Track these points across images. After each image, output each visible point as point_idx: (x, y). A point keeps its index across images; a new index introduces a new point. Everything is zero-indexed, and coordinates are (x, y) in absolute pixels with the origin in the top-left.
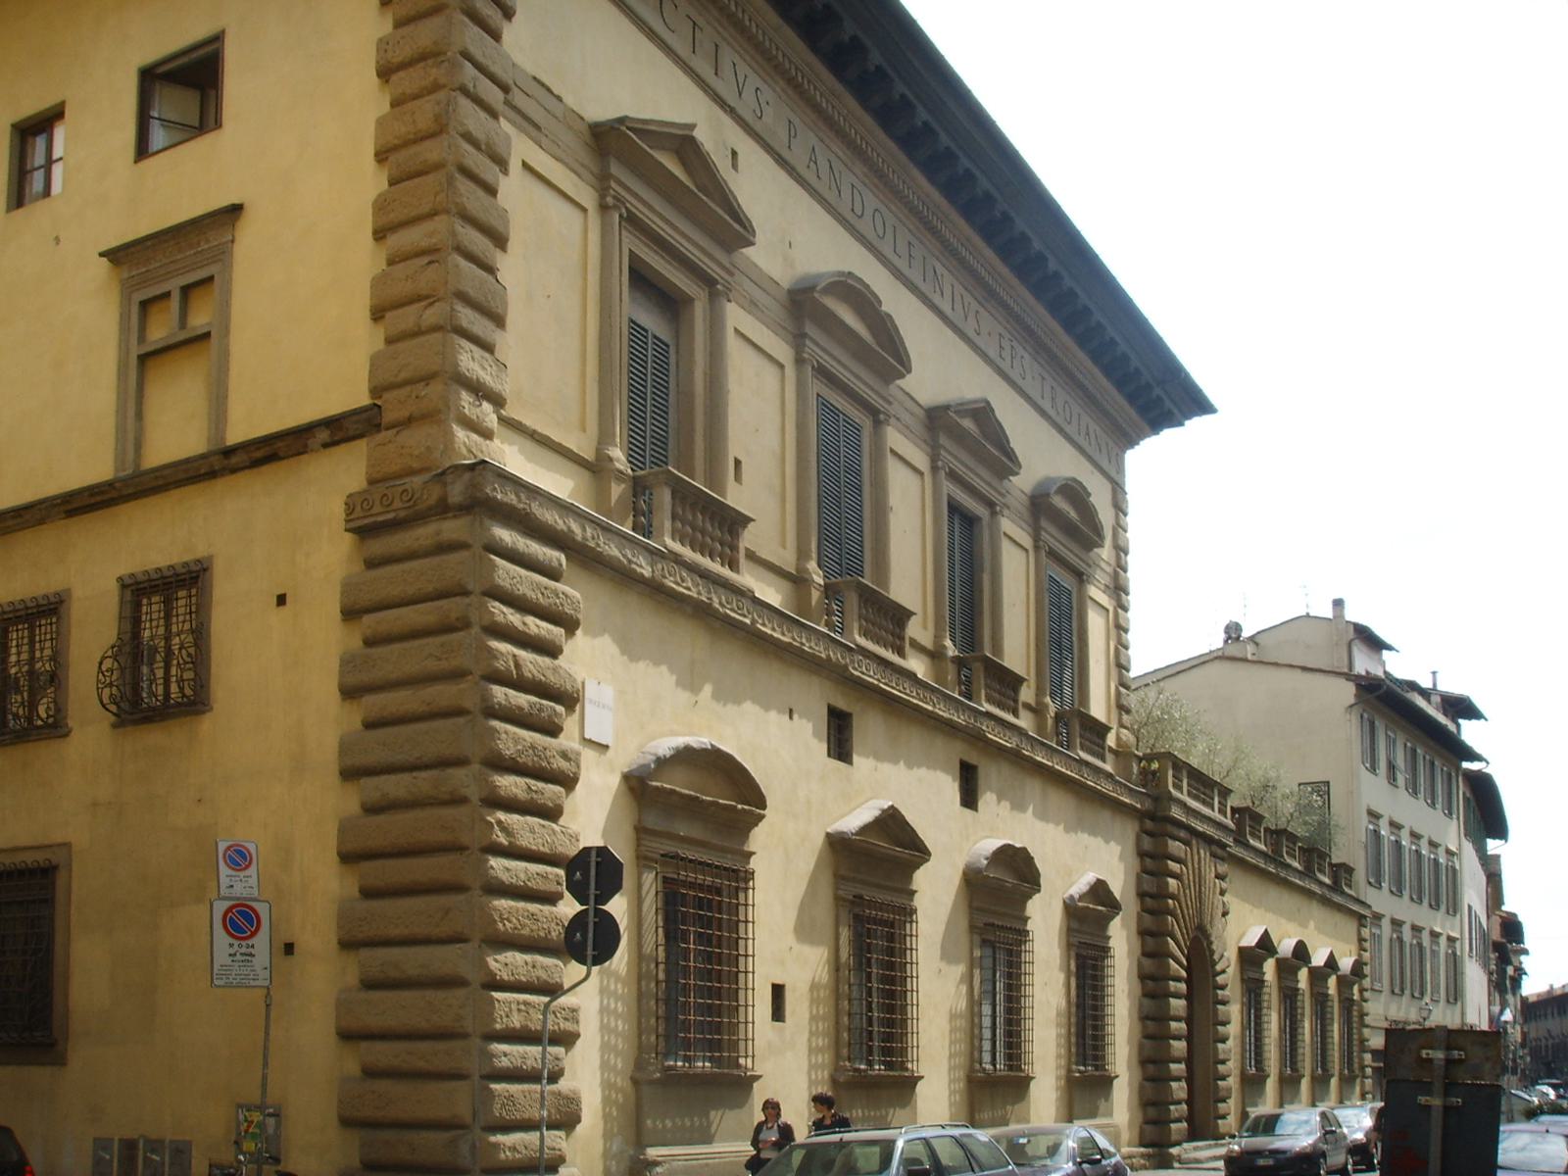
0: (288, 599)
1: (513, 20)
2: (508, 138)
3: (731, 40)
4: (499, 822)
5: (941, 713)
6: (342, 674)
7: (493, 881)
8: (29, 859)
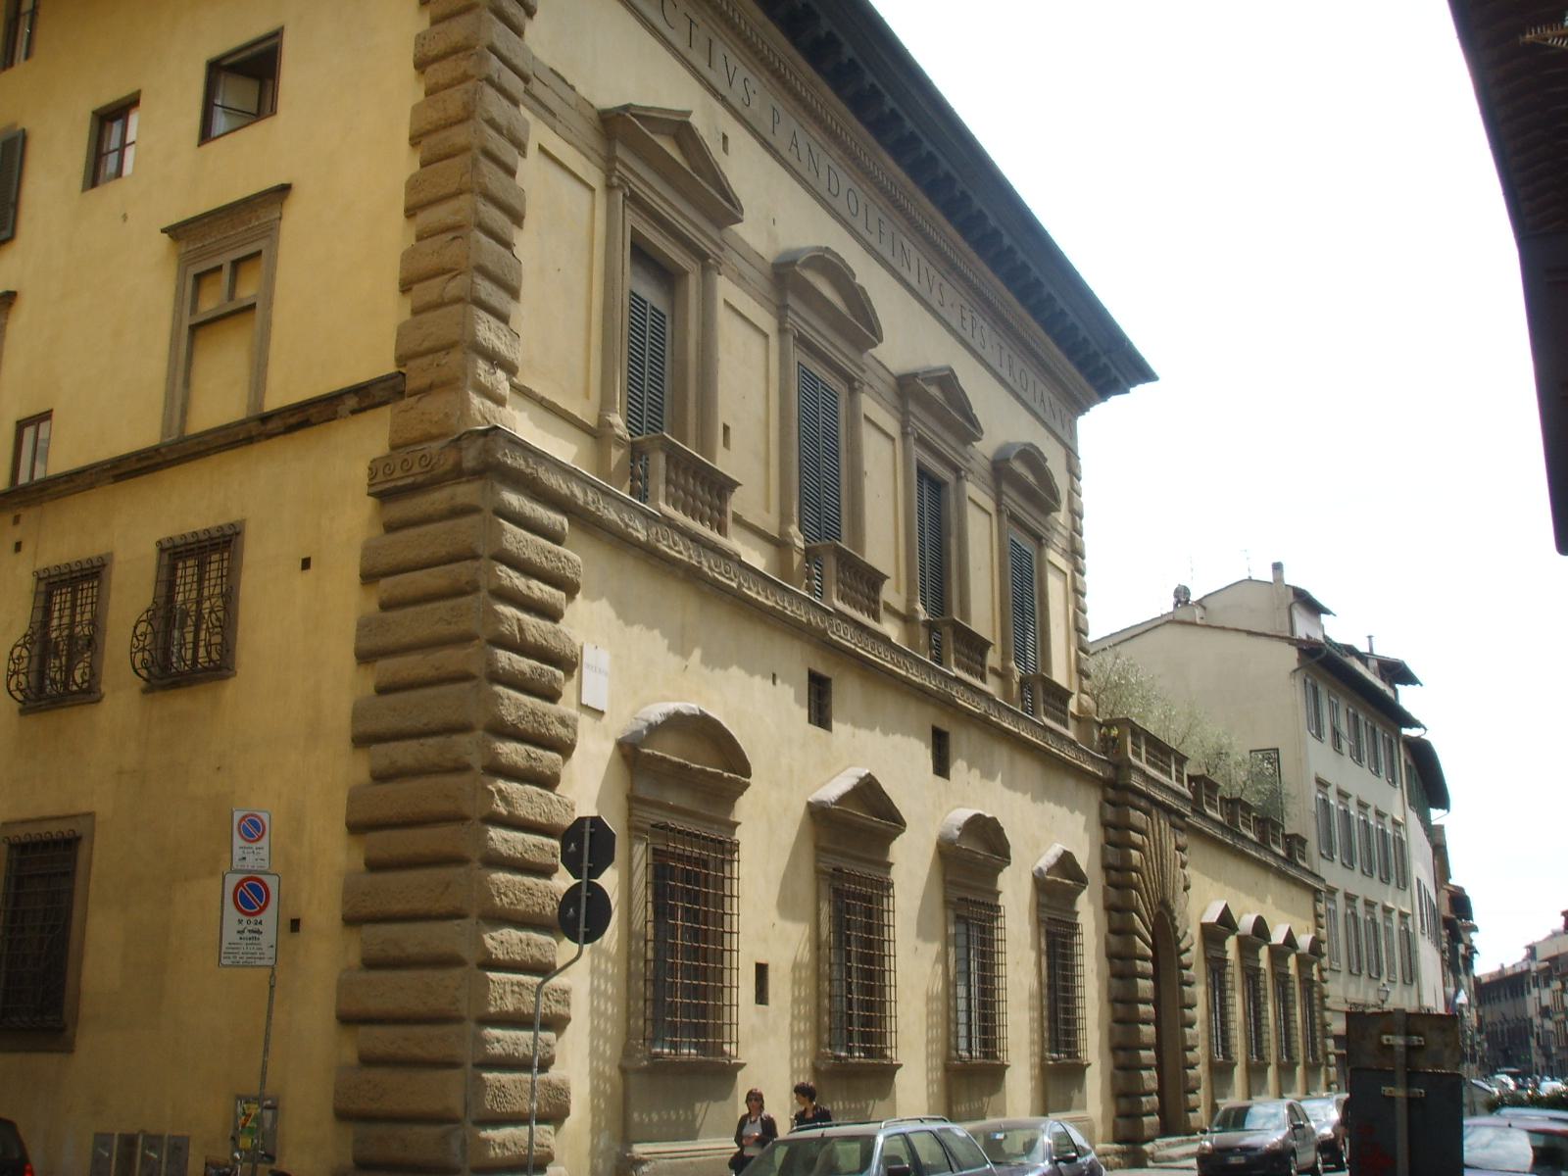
1: (535, 17)
2: (527, 123)
4: (500, 791)
5: (914, 678)
6: (358, 638)
7: (491, 853)
8: (54, 829)
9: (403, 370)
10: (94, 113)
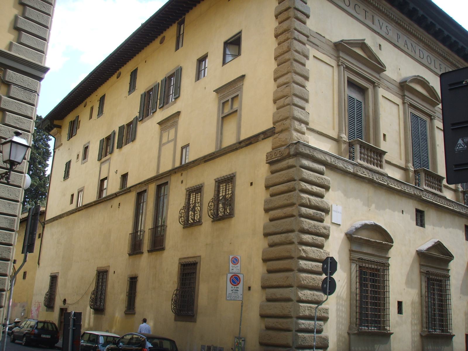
0: (253, 184)
1: (310, 18)
2: (308, 49)
3: (377, 14)
4: (303, 250)
5: (456, 210)
6: (264, 206)
7: (300, 268)
8: (191, 260)
9: (275, 126)
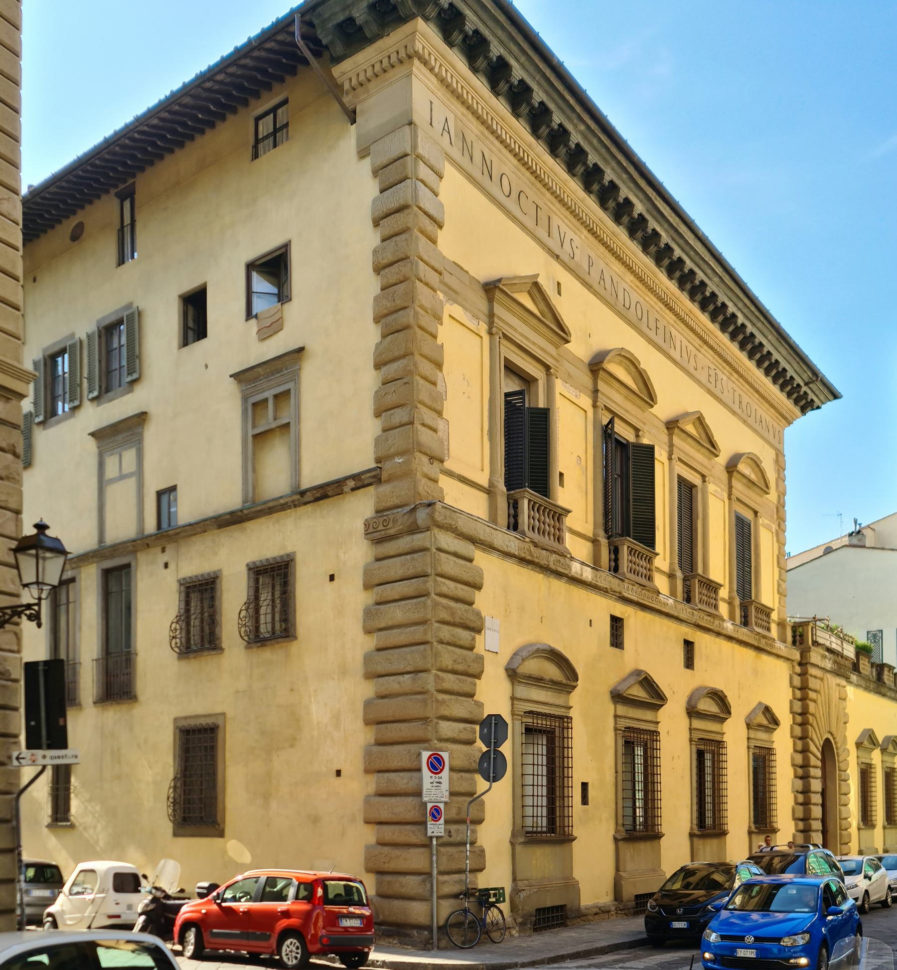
8: (204, 722)
10: (180, 296)
